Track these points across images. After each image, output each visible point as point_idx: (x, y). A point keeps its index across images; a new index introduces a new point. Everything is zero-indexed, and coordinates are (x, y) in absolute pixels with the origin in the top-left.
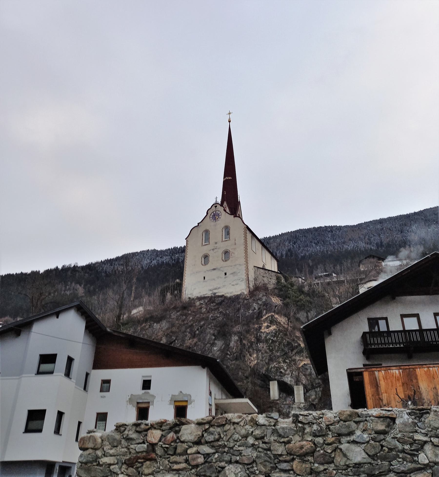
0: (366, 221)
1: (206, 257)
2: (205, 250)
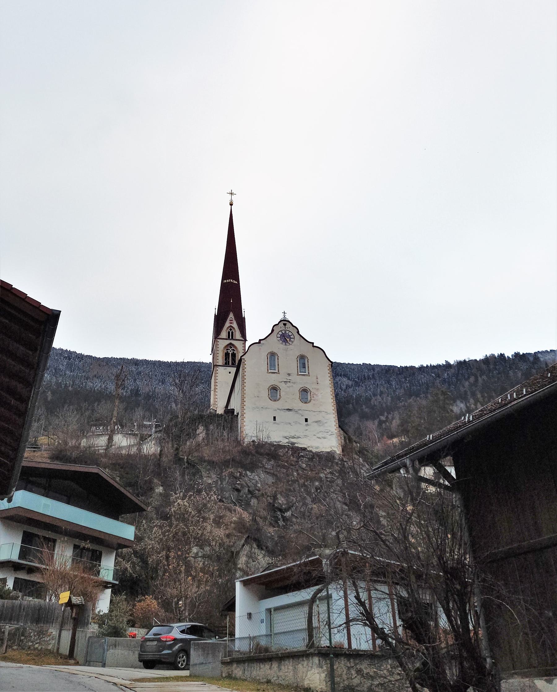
0: (113, 357)
1: (274, 389)
2: (274, 379)
